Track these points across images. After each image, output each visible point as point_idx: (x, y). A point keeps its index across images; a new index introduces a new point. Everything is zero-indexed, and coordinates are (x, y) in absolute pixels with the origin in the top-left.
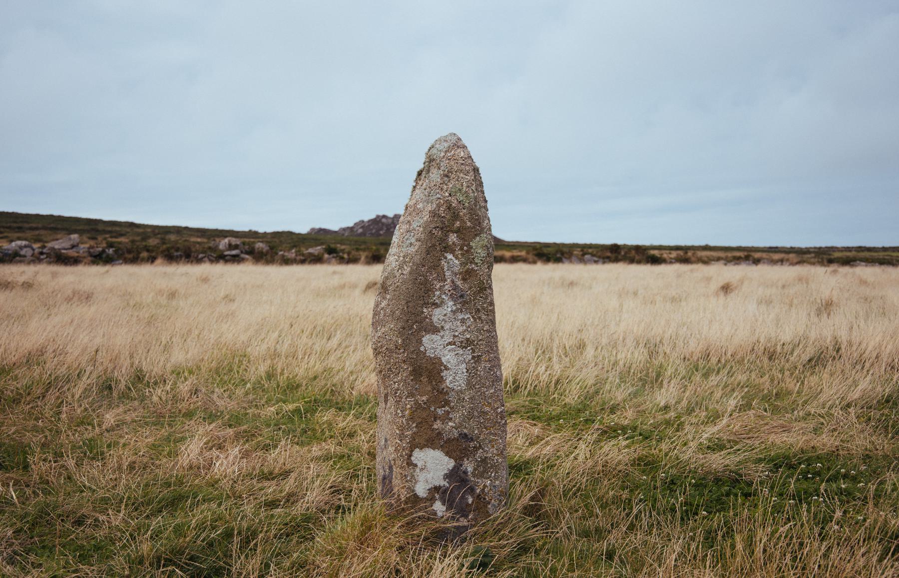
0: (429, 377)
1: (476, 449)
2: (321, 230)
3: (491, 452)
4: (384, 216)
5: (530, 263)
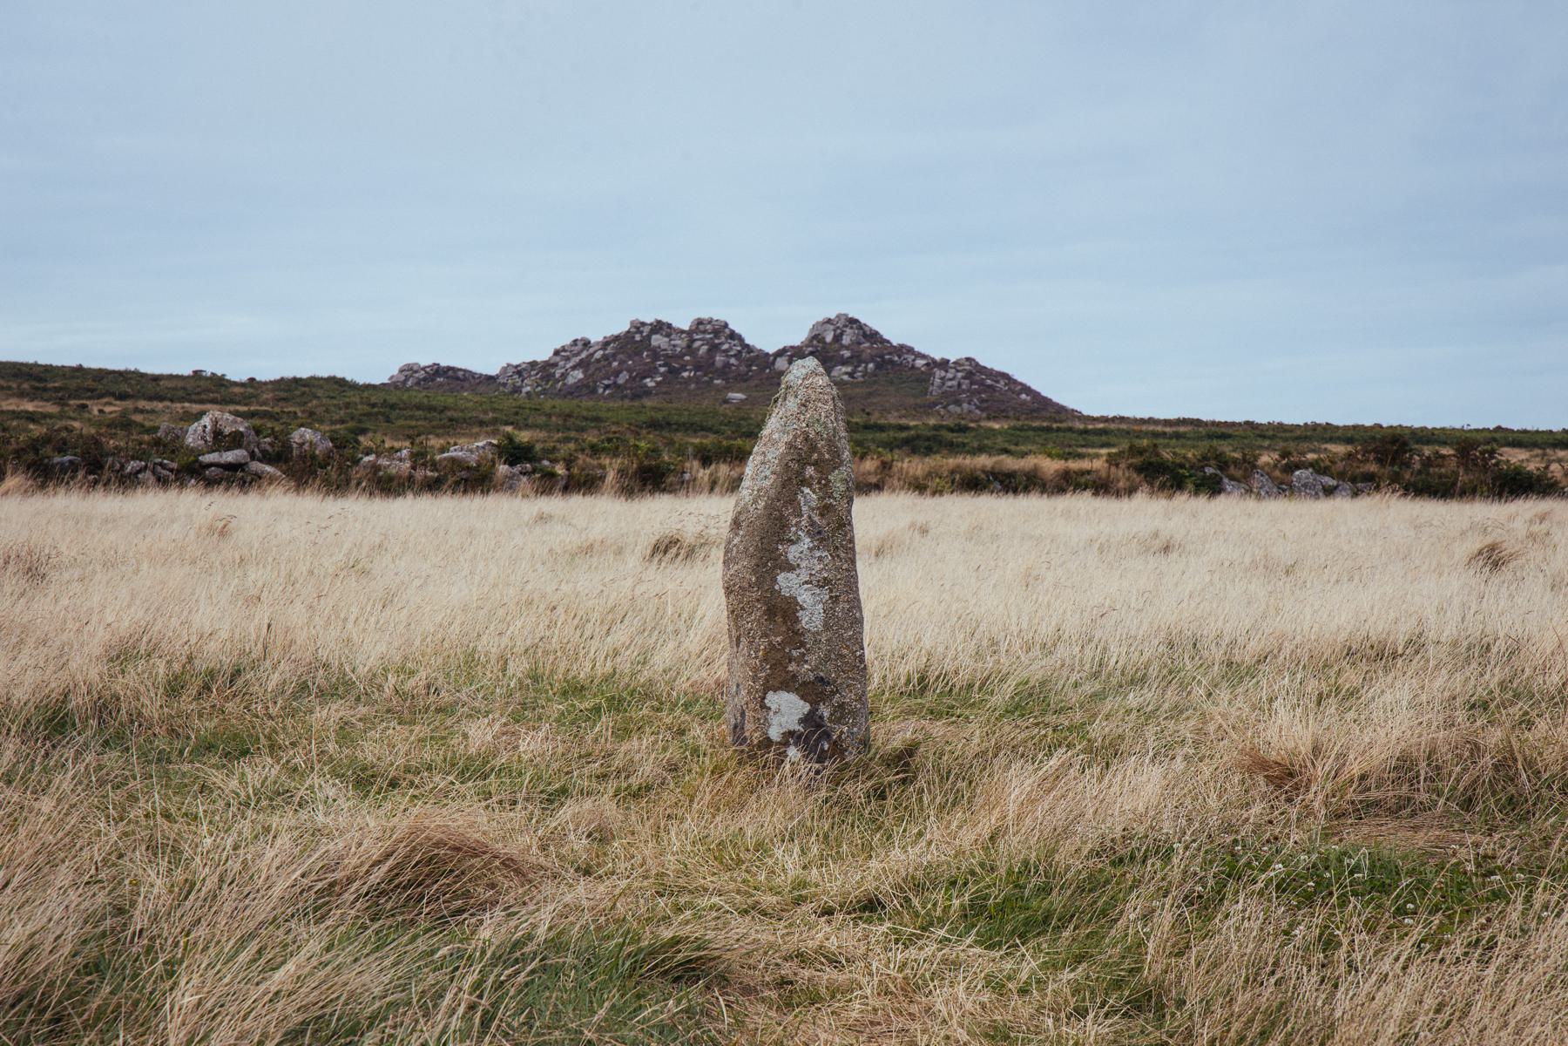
0: (784, 617)
1: (833, 693)
2: (437, 371)
3: (849, 697)
4: (659, 327)
5: (1118, 494)
